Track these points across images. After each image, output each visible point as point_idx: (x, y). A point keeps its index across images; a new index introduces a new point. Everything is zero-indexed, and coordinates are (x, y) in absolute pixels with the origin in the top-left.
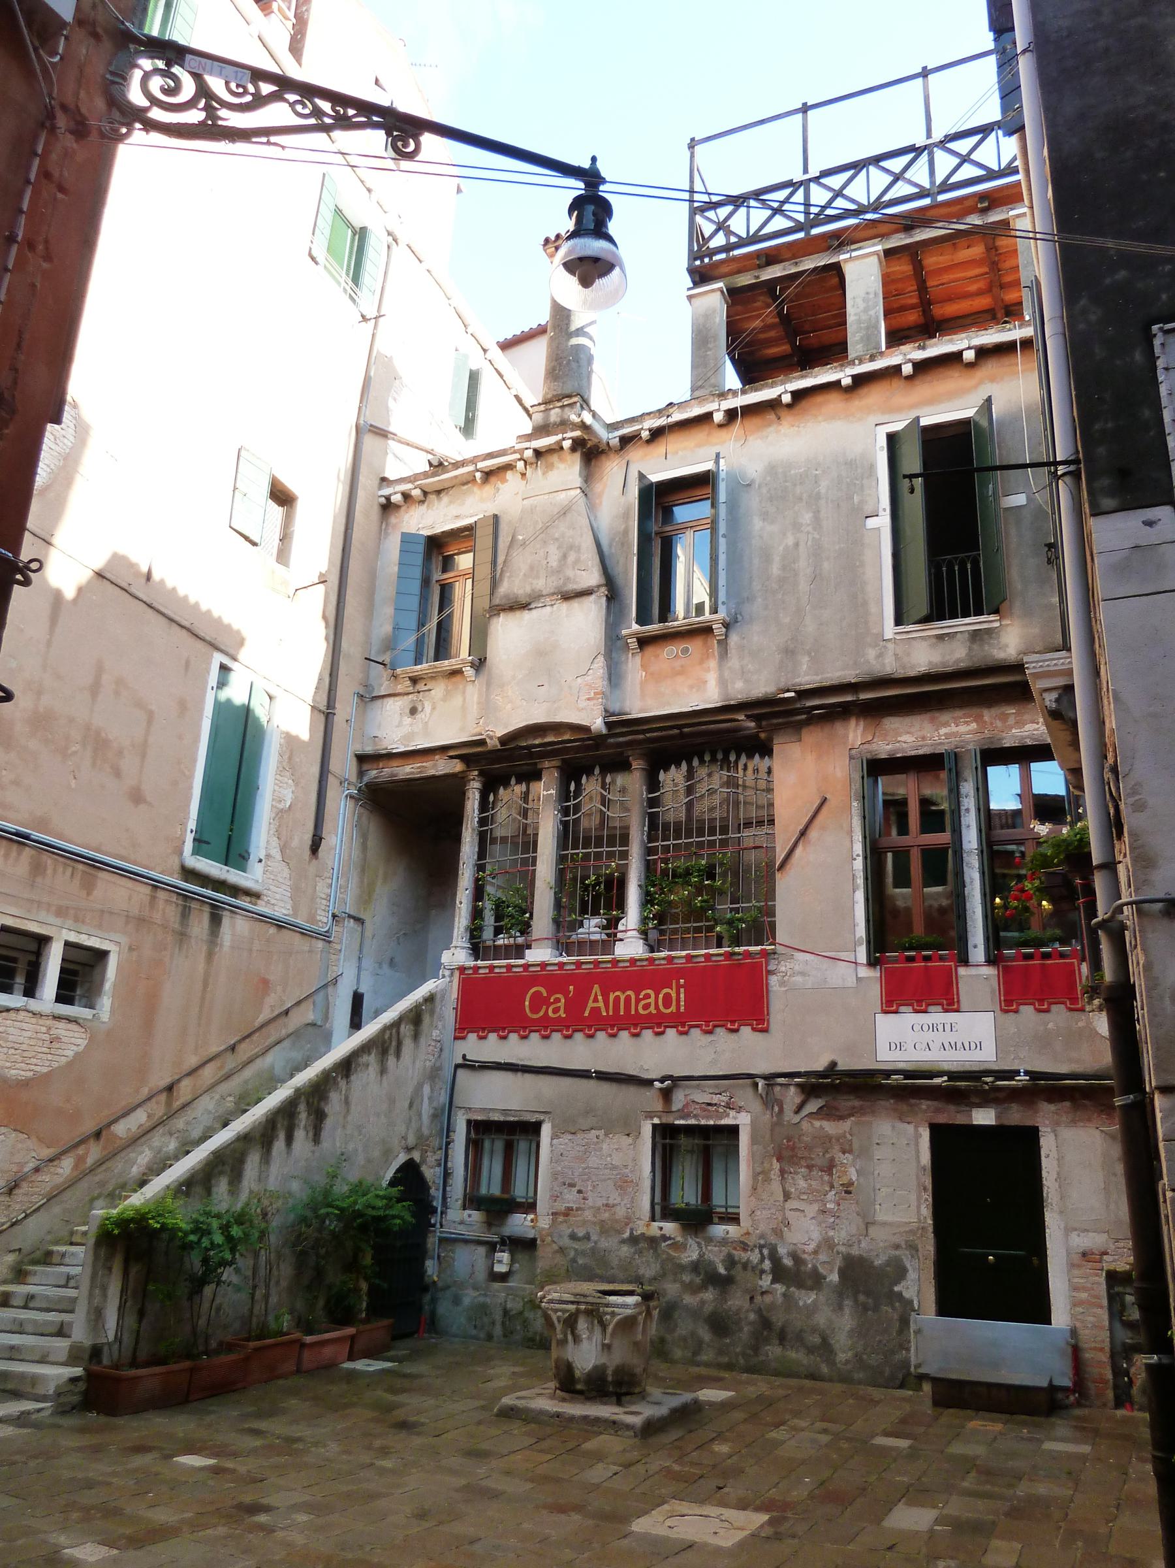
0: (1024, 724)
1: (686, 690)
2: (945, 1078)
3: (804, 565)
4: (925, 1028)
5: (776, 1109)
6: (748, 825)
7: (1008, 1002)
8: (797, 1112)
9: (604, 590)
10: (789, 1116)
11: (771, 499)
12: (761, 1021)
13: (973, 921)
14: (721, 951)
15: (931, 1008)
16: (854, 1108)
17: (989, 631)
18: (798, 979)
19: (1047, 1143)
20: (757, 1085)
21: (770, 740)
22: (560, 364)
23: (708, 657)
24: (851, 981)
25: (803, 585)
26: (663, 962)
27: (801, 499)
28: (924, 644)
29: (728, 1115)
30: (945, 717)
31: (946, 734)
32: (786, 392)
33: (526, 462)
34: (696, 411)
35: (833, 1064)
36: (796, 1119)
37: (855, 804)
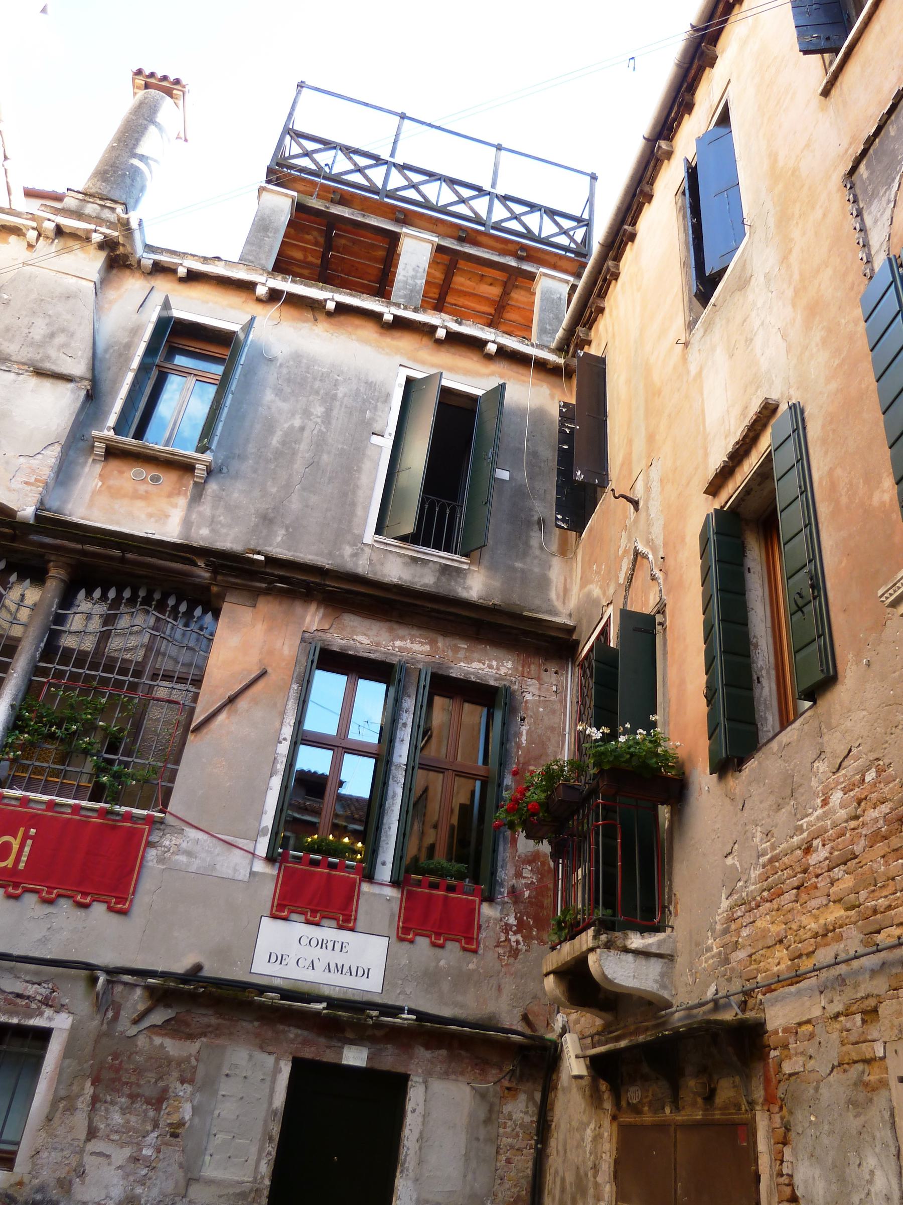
0: (472, 661)
1: (143, 516)
2: (324, 1005)
3: (304, 448)
4: (314, 943)
5: (110, 1014)
6: (167, 677)
7: (406, 930)
8: (136, 1022)
9: (87, 384)
10: (125, 1026)
11: (289, 381)
12: (122, 900)
13: (387, 836)
14: (97, 805)
15: (325, 922)
16: (209, 1026)
17: (458, 571)
18: (183, 858)
19: (415, 1096)
20: (95, 980)
21: (221, 598)
22: (114, 172)
23: (179, 494)
24: (243, 874)
25: (299, 466)
26: (13, 802)
27: (317, 393)
28: (399, 560)
29: (41, 1014)
30: (402, 631)
31: (400, 647)
32: (332, 300)
33: (39, 235)
34: (241, 274)
35: (198, 968)
36: (133, 1031)
37: (295, 686)
